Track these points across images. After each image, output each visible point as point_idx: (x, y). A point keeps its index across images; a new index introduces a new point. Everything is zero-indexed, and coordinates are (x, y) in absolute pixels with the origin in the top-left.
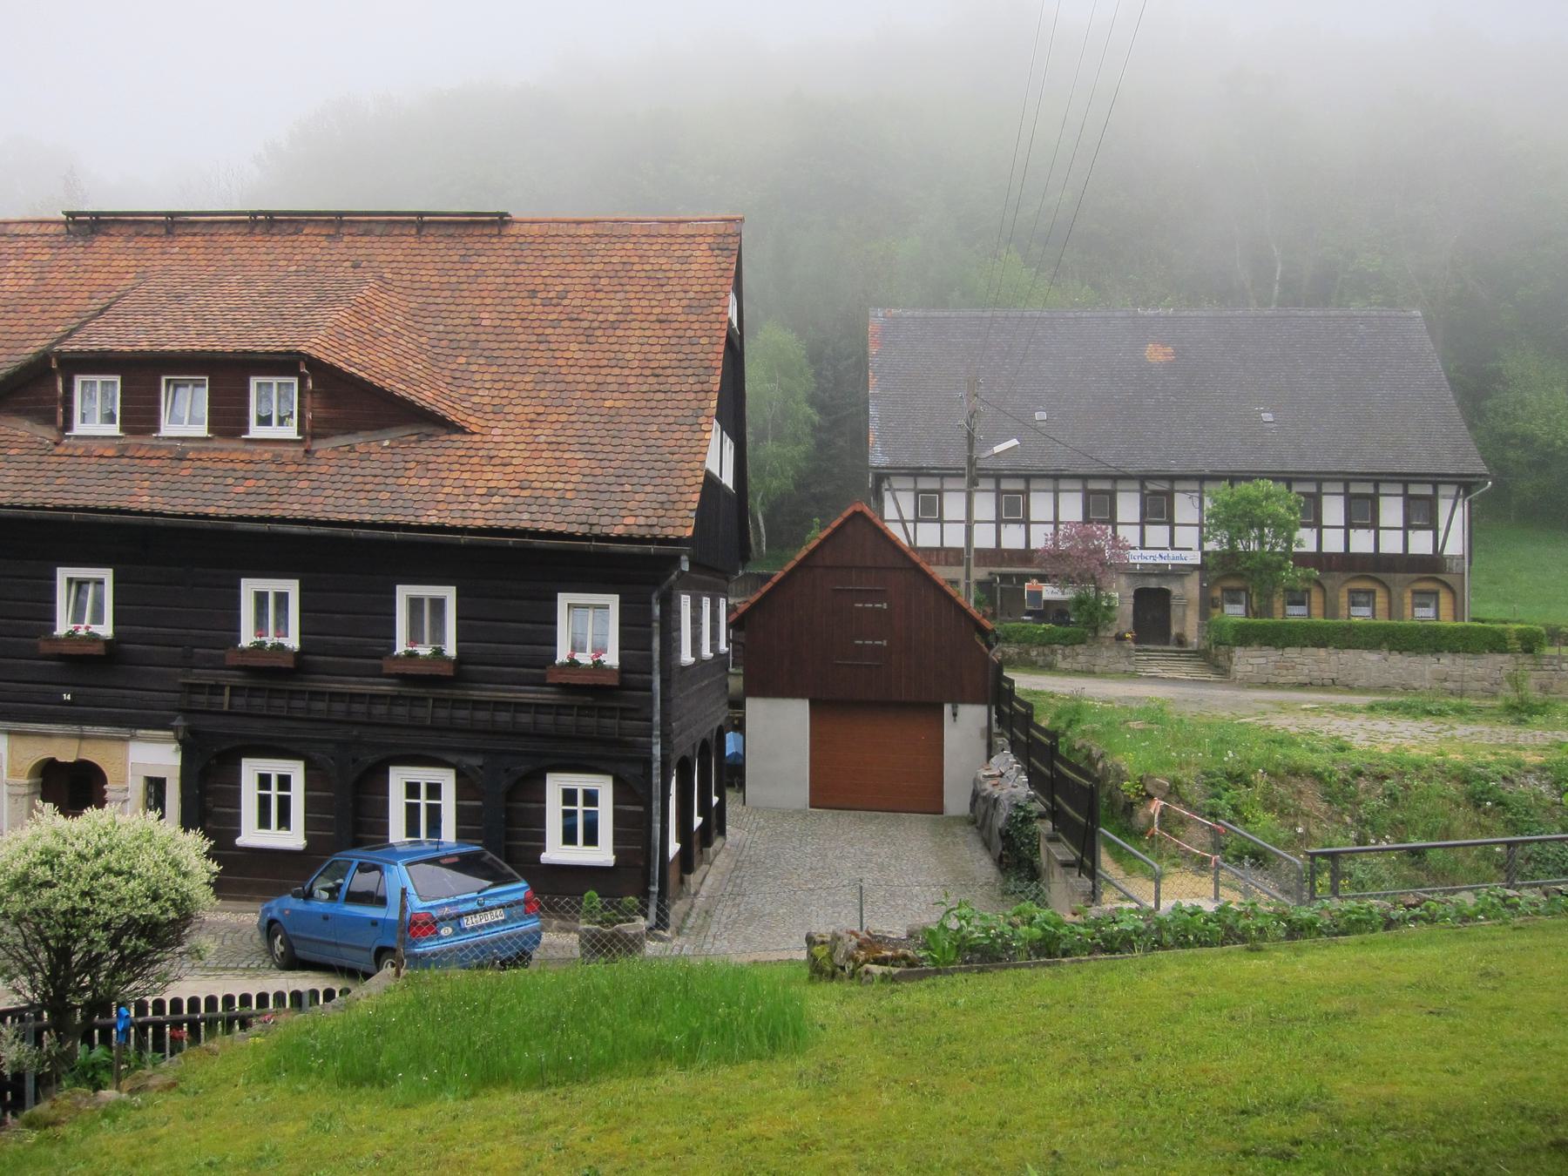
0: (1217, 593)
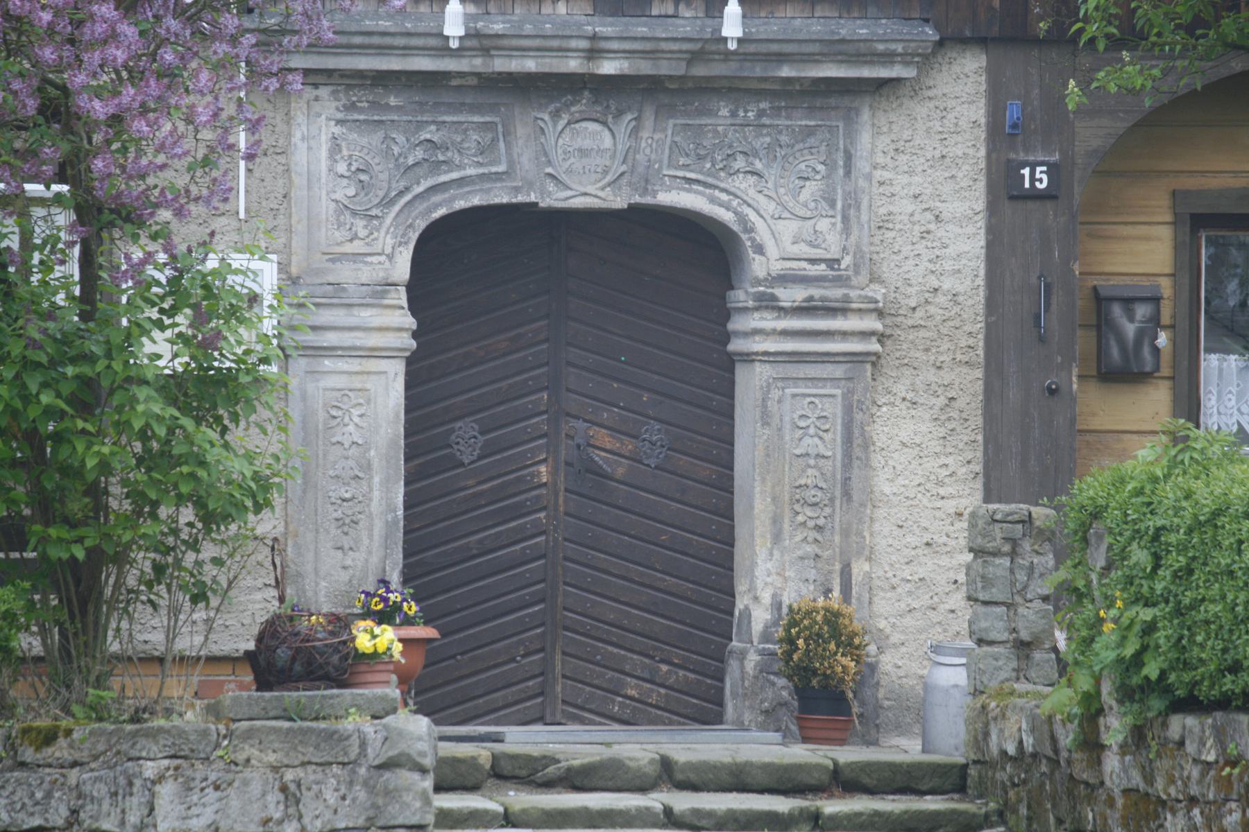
0: (1144, 252)
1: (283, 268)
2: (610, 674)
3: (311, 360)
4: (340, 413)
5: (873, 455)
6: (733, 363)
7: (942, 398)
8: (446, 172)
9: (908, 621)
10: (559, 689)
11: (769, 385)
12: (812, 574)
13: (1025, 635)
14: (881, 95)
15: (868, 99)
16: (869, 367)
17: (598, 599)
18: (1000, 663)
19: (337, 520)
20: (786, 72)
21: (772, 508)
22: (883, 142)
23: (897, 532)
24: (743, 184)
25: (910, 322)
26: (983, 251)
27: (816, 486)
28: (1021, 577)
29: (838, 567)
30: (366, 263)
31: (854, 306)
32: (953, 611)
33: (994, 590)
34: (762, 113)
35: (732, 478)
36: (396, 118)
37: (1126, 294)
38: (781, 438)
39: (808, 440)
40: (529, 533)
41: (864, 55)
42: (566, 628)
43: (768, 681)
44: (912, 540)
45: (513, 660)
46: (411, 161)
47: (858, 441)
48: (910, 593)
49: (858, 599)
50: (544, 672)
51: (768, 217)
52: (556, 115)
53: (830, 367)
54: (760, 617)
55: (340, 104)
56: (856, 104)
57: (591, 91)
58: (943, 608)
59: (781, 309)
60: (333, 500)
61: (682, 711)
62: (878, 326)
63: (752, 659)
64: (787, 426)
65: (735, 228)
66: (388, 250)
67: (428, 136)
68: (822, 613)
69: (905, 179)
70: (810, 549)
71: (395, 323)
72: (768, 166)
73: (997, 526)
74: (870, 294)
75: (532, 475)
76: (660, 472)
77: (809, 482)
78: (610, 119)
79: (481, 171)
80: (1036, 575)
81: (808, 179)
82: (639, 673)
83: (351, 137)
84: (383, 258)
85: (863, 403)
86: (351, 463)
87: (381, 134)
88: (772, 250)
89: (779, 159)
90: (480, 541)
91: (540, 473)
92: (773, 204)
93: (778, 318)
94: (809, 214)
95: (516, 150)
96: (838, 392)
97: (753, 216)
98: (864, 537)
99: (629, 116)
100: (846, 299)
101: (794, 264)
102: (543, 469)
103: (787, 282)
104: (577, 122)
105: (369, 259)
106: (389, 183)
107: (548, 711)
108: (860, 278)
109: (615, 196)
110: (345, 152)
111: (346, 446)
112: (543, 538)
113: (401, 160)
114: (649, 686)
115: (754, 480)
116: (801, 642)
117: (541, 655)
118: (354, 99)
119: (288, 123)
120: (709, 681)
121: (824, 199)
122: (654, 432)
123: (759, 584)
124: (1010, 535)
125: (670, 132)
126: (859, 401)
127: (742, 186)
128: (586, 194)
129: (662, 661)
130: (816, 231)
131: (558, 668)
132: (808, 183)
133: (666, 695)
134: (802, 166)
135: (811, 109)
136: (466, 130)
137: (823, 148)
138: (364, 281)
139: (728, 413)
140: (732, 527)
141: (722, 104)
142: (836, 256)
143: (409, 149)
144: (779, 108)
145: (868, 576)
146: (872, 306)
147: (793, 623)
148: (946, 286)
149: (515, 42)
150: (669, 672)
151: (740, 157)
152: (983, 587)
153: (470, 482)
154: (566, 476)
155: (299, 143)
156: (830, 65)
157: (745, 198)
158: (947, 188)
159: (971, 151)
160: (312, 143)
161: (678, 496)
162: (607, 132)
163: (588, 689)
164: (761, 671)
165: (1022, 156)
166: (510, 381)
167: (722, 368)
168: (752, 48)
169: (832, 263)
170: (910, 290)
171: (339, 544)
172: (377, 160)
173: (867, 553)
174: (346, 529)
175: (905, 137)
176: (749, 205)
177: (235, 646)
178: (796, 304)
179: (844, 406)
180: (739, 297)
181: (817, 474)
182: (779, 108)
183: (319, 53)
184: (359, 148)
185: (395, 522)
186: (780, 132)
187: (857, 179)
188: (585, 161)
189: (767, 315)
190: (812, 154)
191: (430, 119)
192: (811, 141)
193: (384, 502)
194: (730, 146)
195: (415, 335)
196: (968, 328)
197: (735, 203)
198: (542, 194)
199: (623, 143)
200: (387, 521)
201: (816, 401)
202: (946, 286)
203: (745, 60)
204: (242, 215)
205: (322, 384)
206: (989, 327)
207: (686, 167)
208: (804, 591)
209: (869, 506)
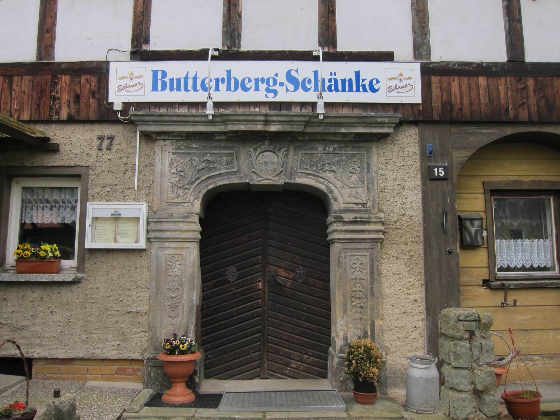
0: (474, 203)
1: (150, 208)
2: (285, 359)
5: (382, 278)
6: (329, 244)
7: (408, 255)
8: (214, 172)
9: (397, 343)
10: (266, 365)
11: (340, 252)
12: (359, 326)
13: (480, 387)
16: (379, 244)
18: (466, 403)
19: (170, 305)
20: (343, 130)
22: (381, 160)
23: (392, 308)
24: (329, 175)
25: (394, 227)
26: (421, 200)
28: (476, 352)
29: (369, 322)
30: (183, 206)
31: (373, 220)
32: (415, 339)
33: (461, 361)
35: (329, 286)
37: (471, 217)
38: (346, 272)
39: (356, 273)
41: (373, 123)
42: (268, 342)
44: (398, 311)
45: (249, 354)
47: (376, 273)
48: (398, 332)
49: (378, 335)
50: (261, 358)
51: (338, 188)
52: (256, 149)
53: (364, 244)
54: (339, 343)
55: (174, 147)
56: (370, 145)
57: (269, 140)
58: (410, 337)
59: (344, 222)
62: (382, 228)
63: (336, 360)
65: (326, 191)
66: (191, 201)
67: (207, 158)
68: (363, 347)
69: (390, 174)
70: (358, 316)
71: (194, 228)
73: (461, 323)
75: (256, 286)
78: (277, 151)
79: (227, 171)
80: (484, 351)
81: (353, 173)
82: (296, 358)
84: (189, 204)
87: (189, 158)
88: (340, 200)
89: (342, 165)
90: (237, 310)
91: (259, 285)
93: (343, 225)
94: (354, 186)
95: (241, 163)
99: (284, 150)
100: (370, 218)
101: (347, 205)
102: (260, 284)
104: (264, 152)
105: (184, 204)
107: (262, 374)
110: (175, 165)
111: (173, 276)
112: (260, 309)
114: (300, 363)
116: (354, 362)
117: (259, 352)
119: (155, 155)
122: (301, 270)
123: (338, 329)
124: (469, 329)
125: (300, 156)
127: (328, 176)
128: (267, 179)
129: (305, 354)
131: (266, 357)
133: (307, 367)
134: (351, 168)
135: (354, 147)
136: (222, 156)
137: (359, 162)
138: (181, 212)
139: (328, 263)
140: (330, 305)
144: (342, 147)
146: (379, 220)
147: (350, 353)
148: (407, 213)
149: (235, 118)
150: (308, 358)
152: (455, 359)
153: (234, 289)
155: (158, 161)
156: (360, 128)
158: (406, 177)
159: (414, 163)
161: (310, 293)
162: (275, 156)
163: (277, 365)
164: (339, 366)
165: (434, 164)
167: (324, 246)
168: (329, 120)
169: (364, 204)
170: (394, 215)
175: (389, 158)
176: (331, 183)
177: (129, 355)
180: (330, 219)
182: (342, 147)
183: (161, 125)
185: (193, 306)
186: (342, 156)
189: (339, 224)
192: (354, 159)
194: (323, 161)
195: (201, 233)
196: (416, 229)
197: (326, 182)
199: (281, 159)
201: (359, 257)
202: (407, 213)
204: (136, 189)
206: (425, 228)
207: (306, 169)
208: (356, 332)
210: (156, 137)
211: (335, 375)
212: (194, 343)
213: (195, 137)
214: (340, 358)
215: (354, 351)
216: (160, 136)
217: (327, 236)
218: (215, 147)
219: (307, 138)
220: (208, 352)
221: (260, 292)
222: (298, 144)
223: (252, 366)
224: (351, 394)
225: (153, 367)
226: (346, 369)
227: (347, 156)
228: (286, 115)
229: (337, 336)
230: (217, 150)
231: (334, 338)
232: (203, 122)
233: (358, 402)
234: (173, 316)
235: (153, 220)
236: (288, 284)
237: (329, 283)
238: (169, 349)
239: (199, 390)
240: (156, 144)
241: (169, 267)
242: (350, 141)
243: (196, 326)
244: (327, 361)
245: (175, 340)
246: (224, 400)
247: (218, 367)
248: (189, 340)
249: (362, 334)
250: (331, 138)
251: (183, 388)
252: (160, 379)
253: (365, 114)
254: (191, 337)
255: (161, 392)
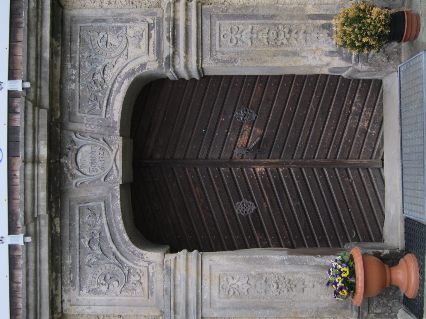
2: (357, 135)
3: (204, 305)
4: (232, 290)
6: (205, 77)
8: (105, 233)
10: (365, 161)
11: (215, 59)
12: (315, 35)
14: (66, 5)
15: (67, 12)
16: (204, 7)
17: (321, 141)
19: (288, 291)
20: (47, 55)
21: (280, 57)
24: (110, 75)
27: (268, 33)
29: (310, 21)
30: (153, 276)
31: (172, 15)
34: (74, 67)
35: (261, 76)
36: (78, 260)
38: (242, 52)
39: (244, 38)
40: (289, 176)
41: (38, 13)
43: (372, 58)
45: (351, 183)
46: (100, 252)
47: (244, 12)
49: (327, 10)
50: (355, 167)
51: (127, 62)
52: (74, 176)
53: (205, 27)
54: (337, 63)
56: (69, 18)
57: (61, 158)
59: (174, 54)
60: (278, 293)
61: (374, 99)
63: (361, 66)
64: (236, 49)
65: (132, 79)
66: (146, 264)
67: (87, 243)
68: (345, 28)
70: (301, 36)
71: (184, 261)
72: (100, 63)
74: (166, 7)
75: (261, 175)
76: (259, 111)
77: (265, 37)
79: (104, 215)
81: (107, 42)
82: (356, 121)
83: (88, 283)
84: (150, 267)
85: (223, 9)
86: (258, 284)
87: (86, 267)
90: (294, 200)
91: (260, 171)
92: (120, 59)
93: (179, 55)
94: (125, 40)
95: (93, 196)
96: (218, 22)
97: (126, 70)
98: (294, 8)
99: (74, 137)
100: (168, 19)
102: (258, 170)
103: (160, 51)
105: (151, 274)
106: (111, 263)
108: (158, 13)
109: (116, 143)
110: (96, 286)
111: (249, 287)
112: (292, 169)
113: (99, 257)
114: (362, 116)
115: (265, 66)
116: (364, 40)
117: (349, 169)
118: (69, 281)
120: (360, 86)
121: (117, 32)
122: (239, 115)
123: (320, 63)
125: (83, 115)
126: (222, 11)
127: (111, 76)
128: (115, 160)
129: (350, 109)
130: (134, 36)
132: (109, 41)
133: (367, 107)
134: (100, 44)
135: (71, 41)
136: (83, 223)
139: (230, 79)
141: (68, 88)
142: (147, 25)
143: (94, 253)
144: (71, 57)
145: (314, 5)
146: (172, 6)
147: (353, 45)
149: (29, 205)
151: (96, 77)
153: (265, 206)
154: (262, 159)
155: (92, 310)
156: (43, 31)
157: (117, 74)
160: (92, 303)
162: (83, 149)
163: (365, 146)
164: (367, 62)
166: (215, 186)
167: (208, 84)
168: (33, 74)
171: (301, 290)
172: (100, 270)
173: (302, 6)
174: (293, 286)
176: (121, 72)
178: (171, 46)
179: (225, 19)
180: (170, 74)
181: (261, 33)
182: (71, 57)
183: (40, 307)
184: (94, 279)
185: (289, 260)
186: (83, 56)
187: (107, 16)
188: (97, 160)
189: (177, 61)
190: (94, 40)
191: (78, 242)
192: (88, 40)
193: (279, 266)
194: (90, 83)
195: (190, 250)
197: (119, 79)
198: (115, 183)
200: (289, 264)
201: (222, 34)
203: (40, 77)
205: (216, 299)
207: (100, 106)
208: (323, 39)
209: (278, 5)
210: (58, 313)
211: (379, 68)
212: (339, 258)
213: (57, 259)
214: (357, 61)
215: (351, 39)
216: (57, 308)
217: (193, 80)
218: (70, 231)
219: (58, 105)
220: (349, 237)
221: (269, 169)
222: (66, 117)
223: (366, 180)
224: (404, 45)
225: (369, 310)
226: (373, 52)
227: (83, 50)
228: (25, 134)
229: (328, 65)
230: (75, 229)
231: (330, 70)
232: (36, 248)
233: (416, 36)
234: (303, 286)
235: (173, 315)
236: (259, 132)
237: (257, 76)
238: (348, 292)
239: (400, 249)
240: (68, 313)
241: (237, 293)
242: (63, 45)
243: (315, 254)
244: (359, 80)
245: (336, 284)
246: (413, 216)
247: (368, 224)
248: (334, 264)
249: (326, 31)
250: (58, 71)
251: (399, 271)
252: (385, 300)
253: (24, 25)
254: (331, 260)
255: (402, 298)
